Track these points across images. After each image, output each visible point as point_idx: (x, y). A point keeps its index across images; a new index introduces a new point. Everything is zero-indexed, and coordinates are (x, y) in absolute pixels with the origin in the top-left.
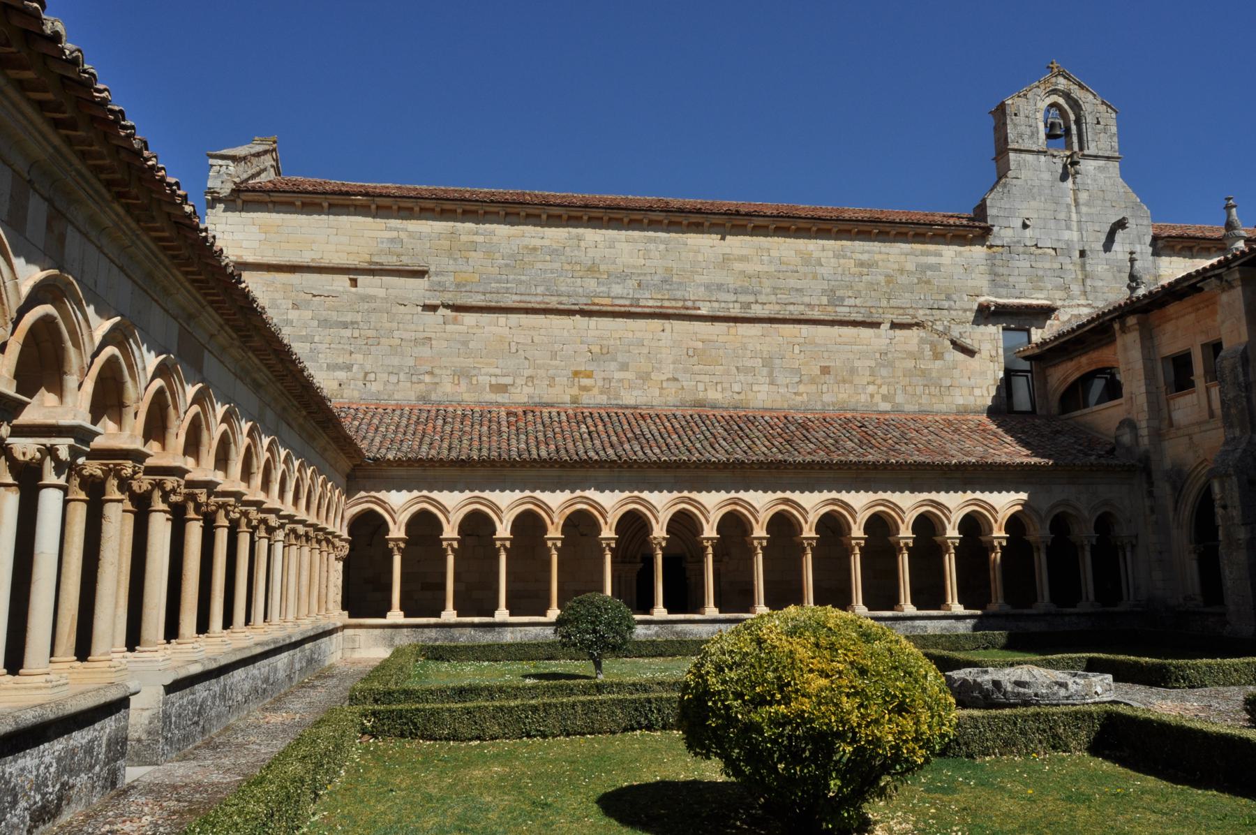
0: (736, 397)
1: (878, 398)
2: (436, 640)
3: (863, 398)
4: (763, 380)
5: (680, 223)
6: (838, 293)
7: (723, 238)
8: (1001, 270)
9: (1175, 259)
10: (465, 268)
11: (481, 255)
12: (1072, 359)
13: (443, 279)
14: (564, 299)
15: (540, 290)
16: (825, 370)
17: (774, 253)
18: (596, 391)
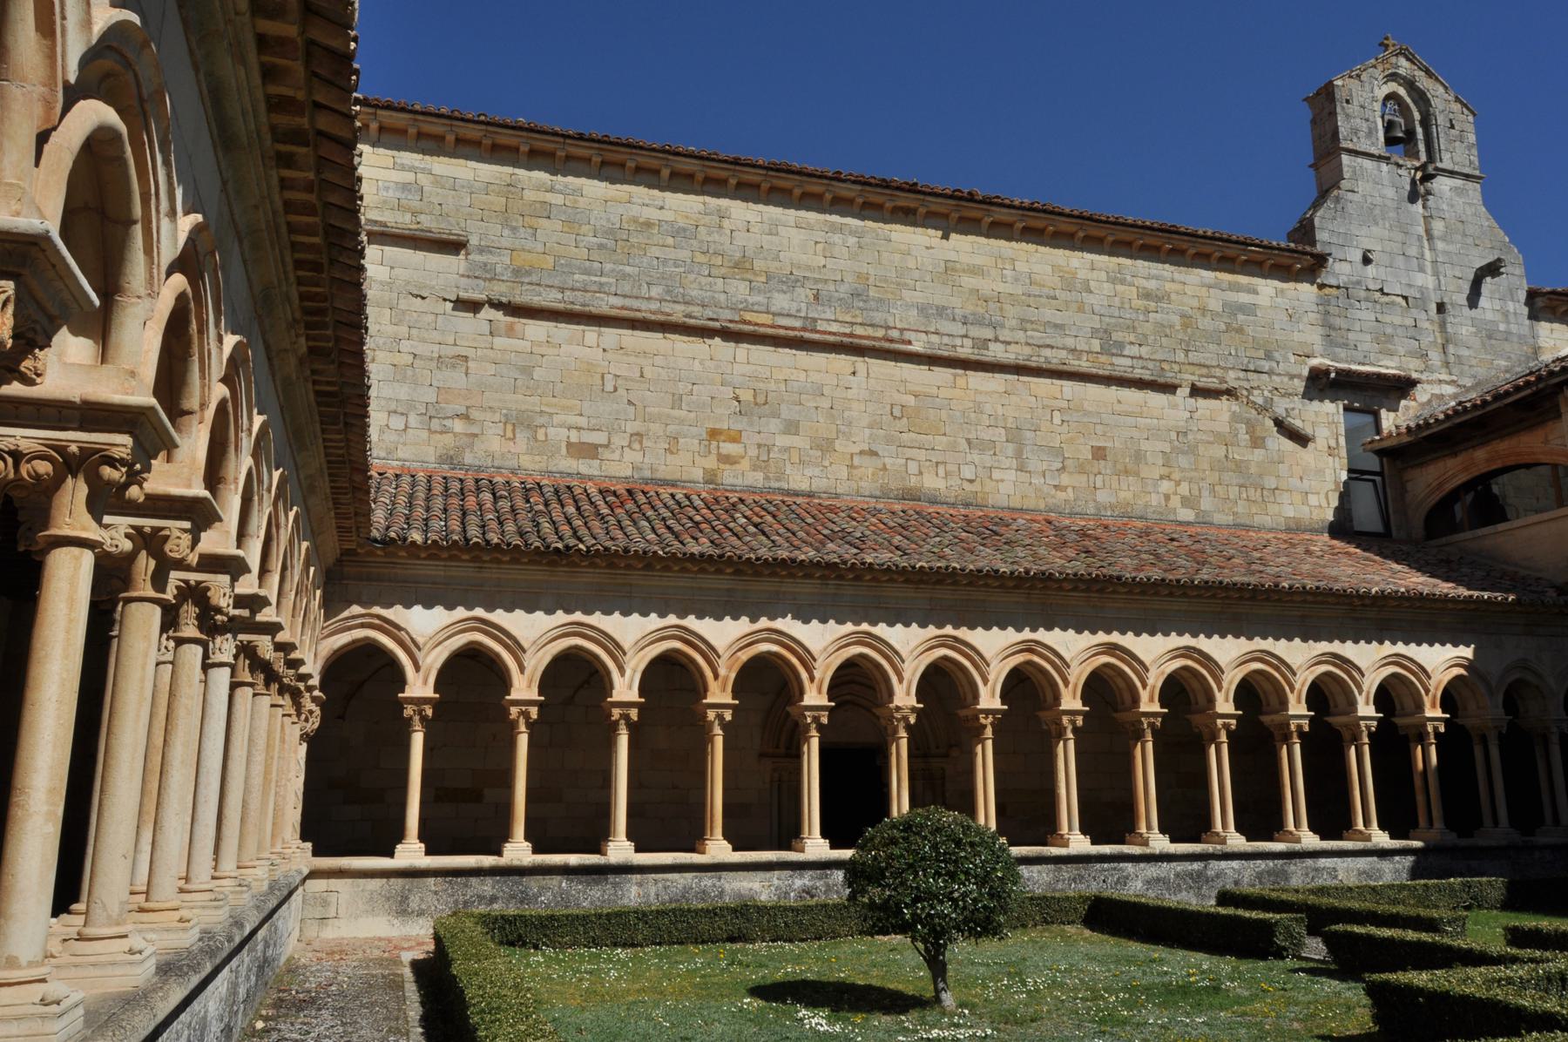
0: (966, 486)
1: (1175, 502)
2: (493, 899)
3: (1155, 500)
4: (1007, 463)
6: (1115, 336)
7: (946, 237)
8: (1338, 322)
9: (1556, 326)
10: (529, 245)
11: (558, 225)
12: (1455, 454)
13: (492, 259)
15: (656, 291)
16: (1099, 453)
17: (1021, 267)
18: (745, 464)
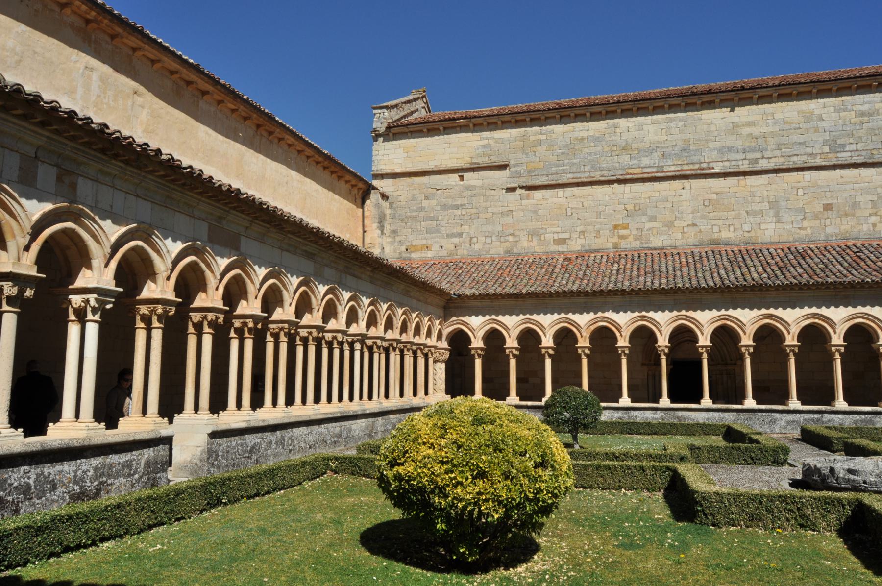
0: (746, 235)
3: (865, 228)
4: (770, 220)
5: (695, 104)
7: (732, 110)
11: (544, 148)
14: (605, 173)
15: (587, 168)
16: (828, 207)
18: (631, 238)
